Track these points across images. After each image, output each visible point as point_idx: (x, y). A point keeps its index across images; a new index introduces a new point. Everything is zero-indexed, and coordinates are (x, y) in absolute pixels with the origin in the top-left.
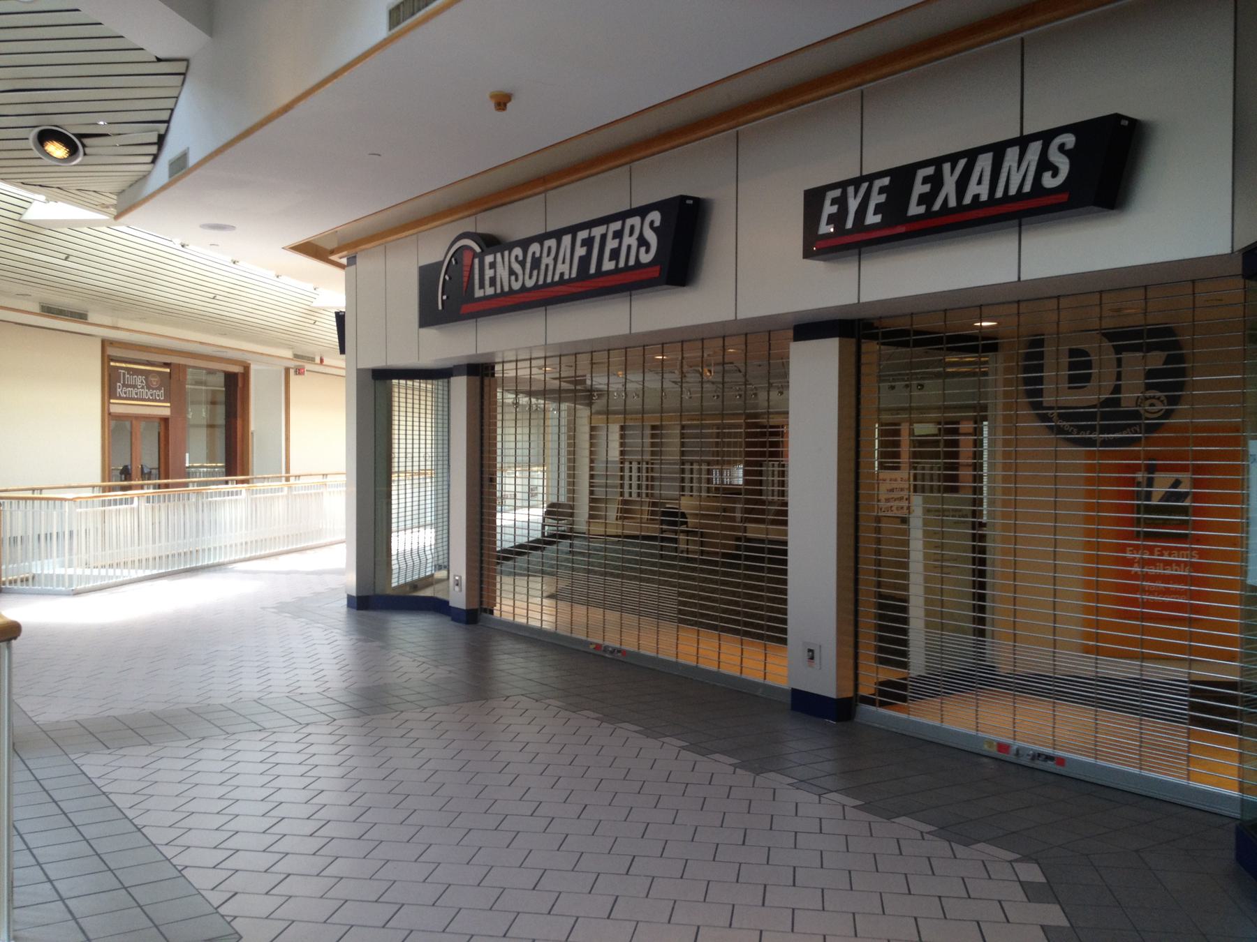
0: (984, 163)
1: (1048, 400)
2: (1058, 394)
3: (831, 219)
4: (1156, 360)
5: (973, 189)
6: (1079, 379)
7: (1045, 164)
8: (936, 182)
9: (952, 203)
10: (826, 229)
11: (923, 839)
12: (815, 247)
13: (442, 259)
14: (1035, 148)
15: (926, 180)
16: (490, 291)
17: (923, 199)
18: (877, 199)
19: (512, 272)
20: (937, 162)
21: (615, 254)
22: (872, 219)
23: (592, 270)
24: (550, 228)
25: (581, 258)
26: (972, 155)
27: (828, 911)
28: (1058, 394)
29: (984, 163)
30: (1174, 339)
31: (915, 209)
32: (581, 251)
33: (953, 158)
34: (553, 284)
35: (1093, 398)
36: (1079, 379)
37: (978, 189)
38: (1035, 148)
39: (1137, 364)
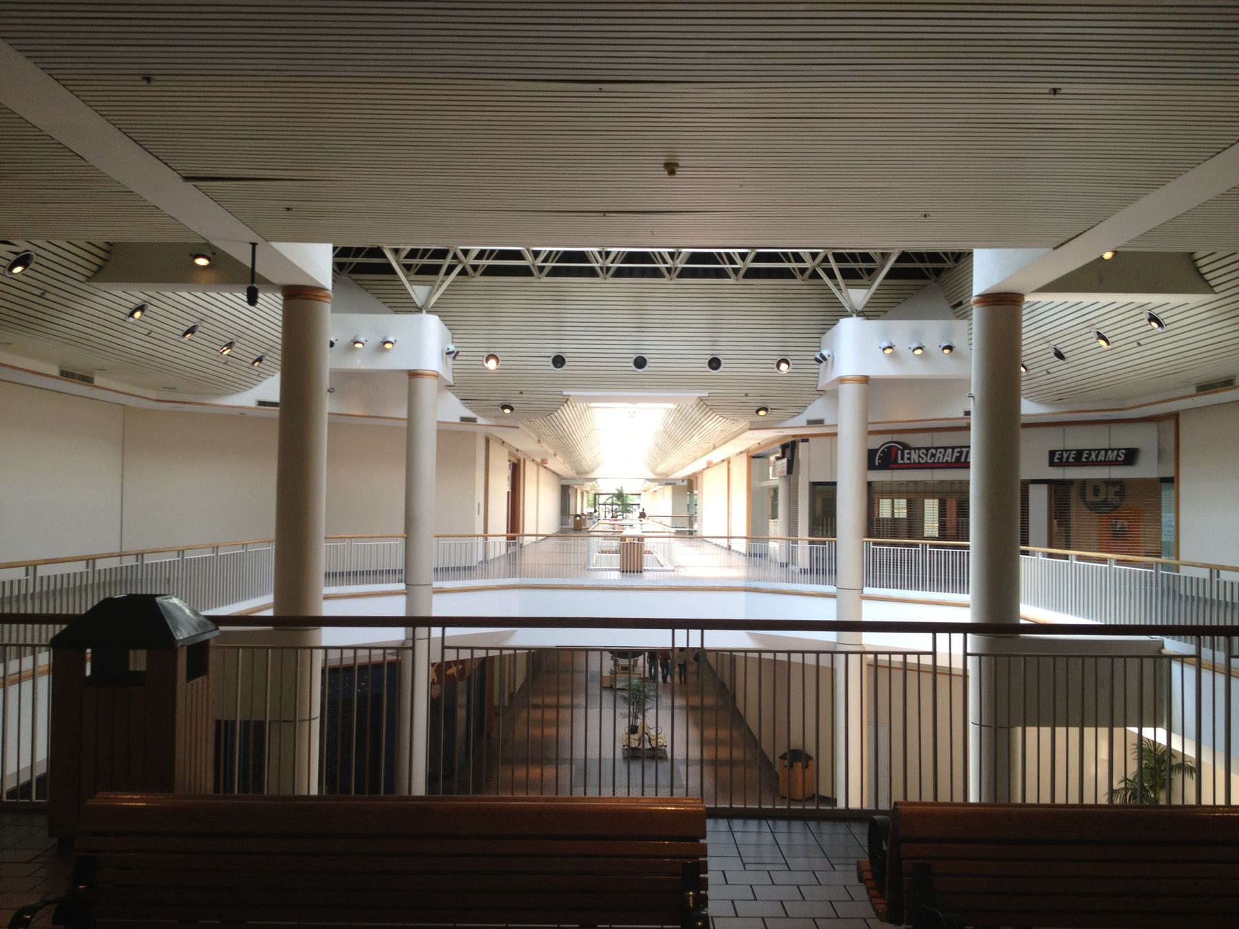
0: (1103, 452)
1: (1087, 500)
2: (1090, 497)
3: (1058, 459)
4: (1117, 488)
5: (946, 458)
6: (1096, 495)
7: (1118, 455)
8: (1090, 455)
9: (1103, 459)
10: (1056, 460)
11: (835, 870)
12: (1052, 464)
13: (877, 447)
14: (1116, 452)
15: (958, 452)
16: (908, 462)
17: (1086, 458)
18: (1072, 456)
19: (920, 457)
20: (1090, 450)
21: (909, 459)
22: (1071, 460)
23: (963, 460)
24: (935, 446)
25: (957, 457)
26: (1100, 450)
27: (826, 901)
28: (1090, 497)
29: (1103, 452)
30: (369, 699)
31: (1084, 460)
32: (956, 454)
33: (1094, 450)
34: (942, 463)
35: (1098, 500)
36: (1096, 495)
37: (1101, 458)
38: (1116, 452)
39: (1113, 490)
